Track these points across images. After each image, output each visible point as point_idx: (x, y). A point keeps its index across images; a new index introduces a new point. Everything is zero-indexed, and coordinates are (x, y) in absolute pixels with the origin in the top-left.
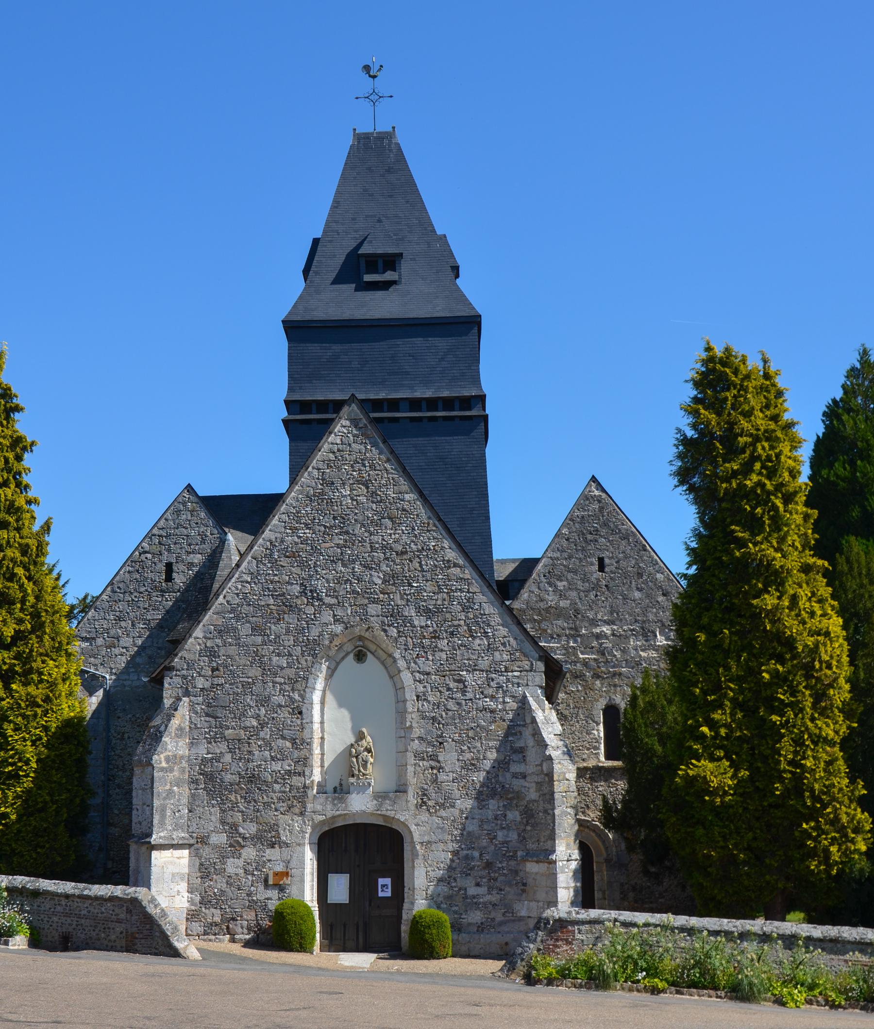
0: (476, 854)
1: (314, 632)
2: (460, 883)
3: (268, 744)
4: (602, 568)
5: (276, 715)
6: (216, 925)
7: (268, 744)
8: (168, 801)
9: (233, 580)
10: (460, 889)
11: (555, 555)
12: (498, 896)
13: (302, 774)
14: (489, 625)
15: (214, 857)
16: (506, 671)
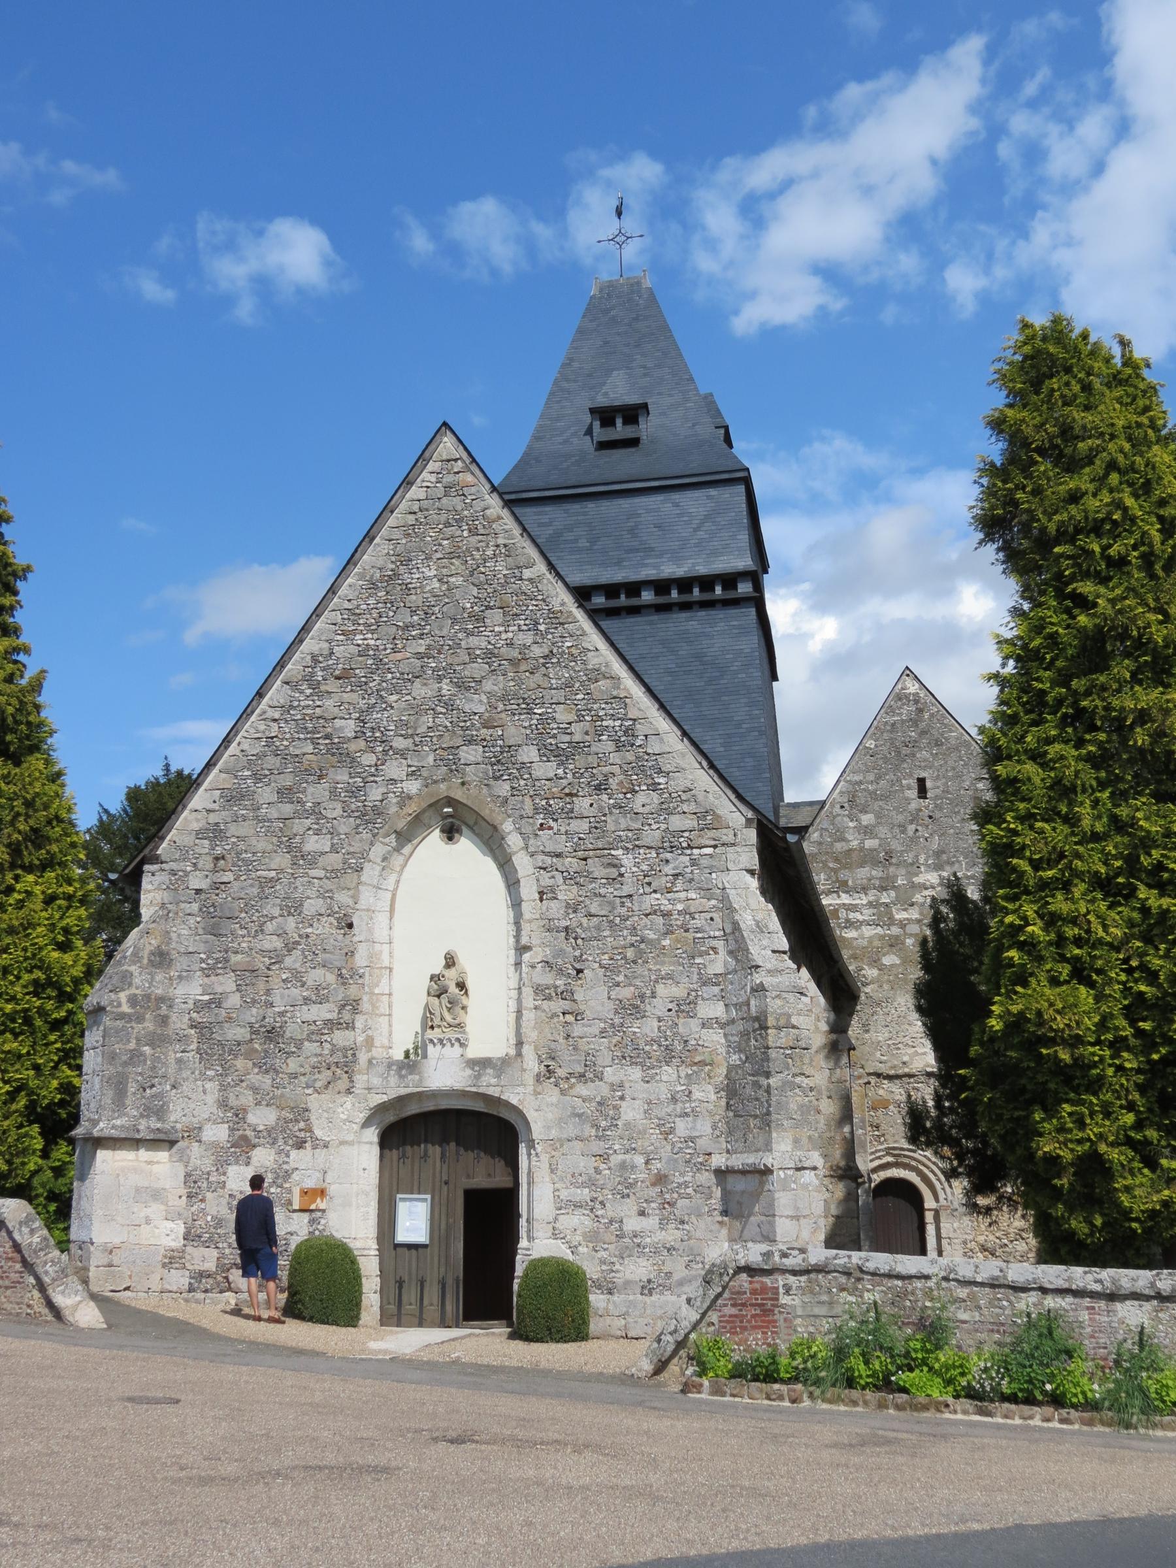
0: (640, 1160)
1: (375, 794)
2: (611, 1211)
3: (297, 978)
4: (922, 791)
5: (309, 930)
6: (209, 1276)
7: (297, 978)
8: (130, 1069)
9: (253, 718)
10: (611, 1222)
11: (857, 778)
12: (678, 1234)
13: (350, 1026)
14: (660, 771)
15: (207, 1164)
16: (690, 847)
